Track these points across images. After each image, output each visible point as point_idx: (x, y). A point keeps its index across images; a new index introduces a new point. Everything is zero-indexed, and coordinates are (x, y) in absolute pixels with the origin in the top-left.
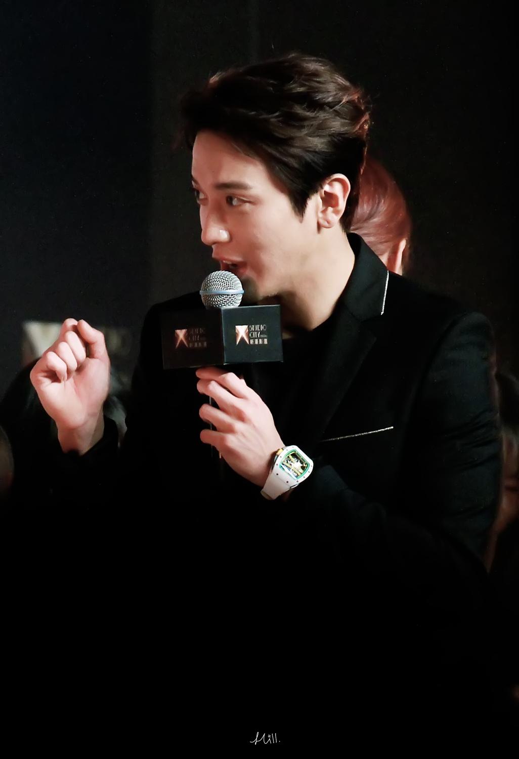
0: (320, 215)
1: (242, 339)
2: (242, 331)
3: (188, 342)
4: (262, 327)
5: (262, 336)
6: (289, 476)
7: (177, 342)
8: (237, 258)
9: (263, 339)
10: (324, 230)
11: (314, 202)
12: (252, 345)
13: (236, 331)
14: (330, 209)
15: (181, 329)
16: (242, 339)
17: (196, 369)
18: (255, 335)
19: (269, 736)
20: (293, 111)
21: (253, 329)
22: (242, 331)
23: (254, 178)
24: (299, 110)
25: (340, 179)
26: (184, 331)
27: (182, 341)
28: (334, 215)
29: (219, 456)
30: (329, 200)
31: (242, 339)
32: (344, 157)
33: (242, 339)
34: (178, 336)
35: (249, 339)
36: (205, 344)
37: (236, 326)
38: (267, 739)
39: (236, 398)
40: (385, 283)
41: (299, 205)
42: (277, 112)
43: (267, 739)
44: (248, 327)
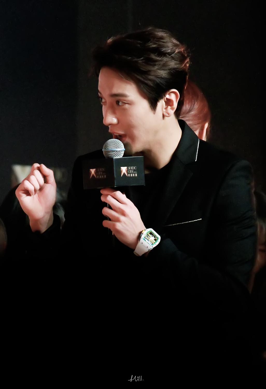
0: (164, 110)
1: (124, 174)
2: (124, 169)
3: (97, 175)
4: (134, 168)
5: (134, 172)
6: (148, 244)
7: (91, 176)
8: (121, 132)
9: (135, 174)
10: (166, 118)
11: (161, 104)
12: (129, 177)
13: (121, 170)
14: (169, 107)
15: (93, 168)
16: (124, 174)
17: (100, 189)
18: (131, 171)
19: (138, 377)
20: (150, 57)
21: (129, 169)
22: (124, 169)
23: (130, 91)
24: (153, 56)
25: (174, 92)
26: (94, 170)
27: (93, 175)
28: (171, 110)
29: (112, 234)
30: (169, 102)
31: (124, 174)
32: (176, 80)
33: (124, 174)
34: (91, 172)
35: (128, 174)
36: (105, 176)
37: (121, 167)
38: (137, 379)
39: (121, 204)
40: (198, 145)
41: (153, 105)
42: (142, 57)
43: (137, 379)
44: (127, 167)
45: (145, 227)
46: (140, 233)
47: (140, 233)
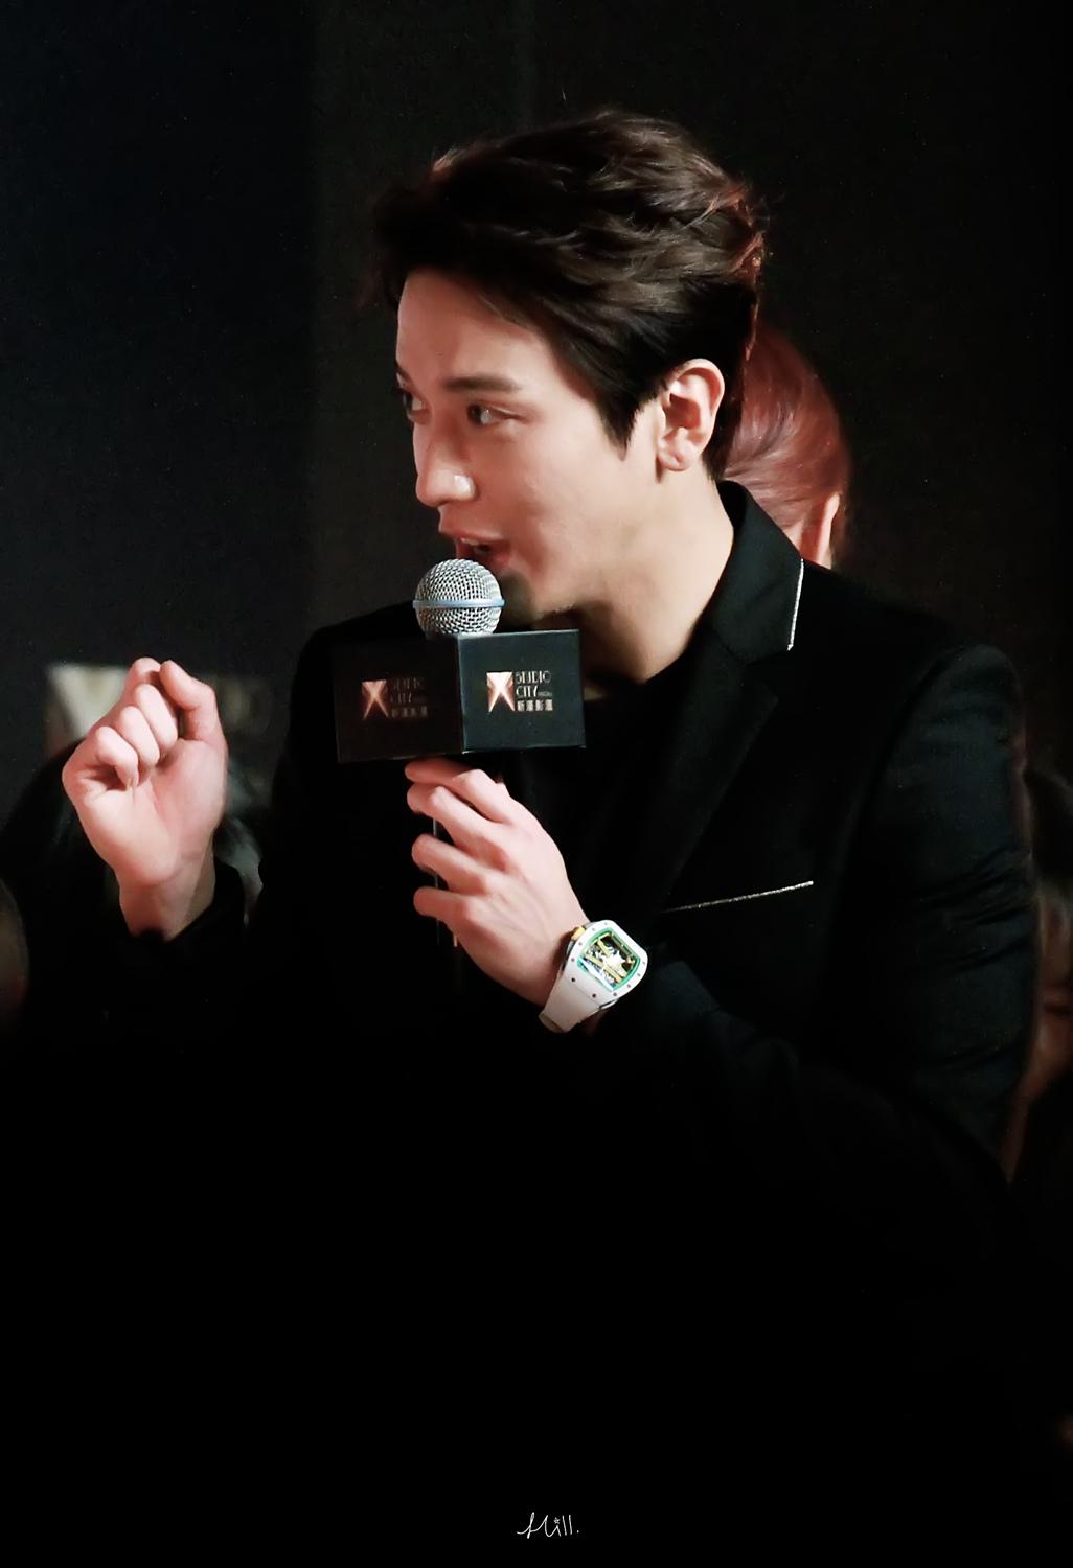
0: (663, 444)
1: (501, 700)
2: (500, 683)
3: (390, 707)
4: (542, 676)
5: (541, 694)
6: (597, 984)
7: (366, 708)
8: (490, 534)
9: (544, 700)
10: (669, 475)
11: (650, 418)
12: (520, 713)
13: (489, 684)
14: (683, 432)
15: (374, 679)
16: (501, 700)
17: (405, 763)
18: (527, 691)
19: (557, 1521)
20: (606, 229)
21: (522, 679)
22: (500, 683)
23: (526, 368)
24: (619, 228)
25: (702, 369)
26: (380, 683)
27: (375, 705)
28: (690, 444)
29: (453, 943)
30: (681, 413)
31: (501, 701)
32: (712, 324)
33: (501, 701)
34: (368, 694)
35: (516, 700)
36: (424, 711)
37: (488, 674)
38: (551, 1526)
39: (489, 822)
40: (797, 586)
41: (619, 423)
42: (572, 231)
43: (551, 1526)
44: (514, 675)
45: (584, 915)
46: (567, 940)
47: (567, 940)
